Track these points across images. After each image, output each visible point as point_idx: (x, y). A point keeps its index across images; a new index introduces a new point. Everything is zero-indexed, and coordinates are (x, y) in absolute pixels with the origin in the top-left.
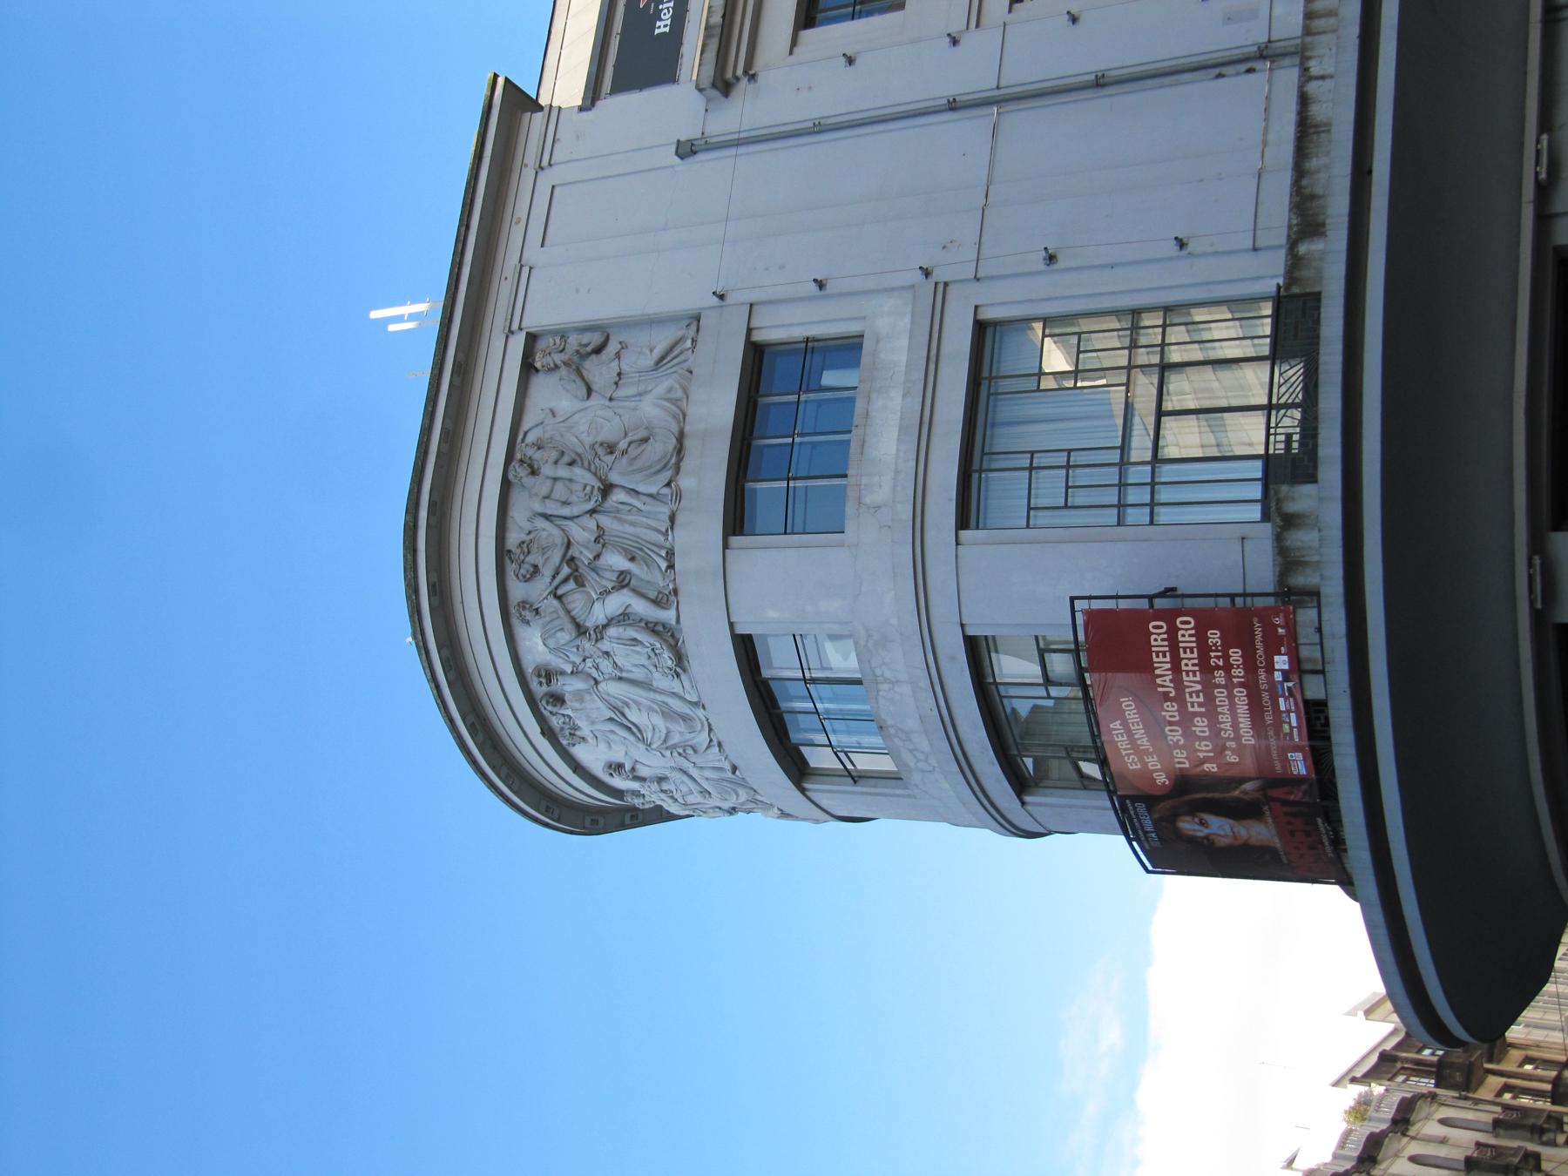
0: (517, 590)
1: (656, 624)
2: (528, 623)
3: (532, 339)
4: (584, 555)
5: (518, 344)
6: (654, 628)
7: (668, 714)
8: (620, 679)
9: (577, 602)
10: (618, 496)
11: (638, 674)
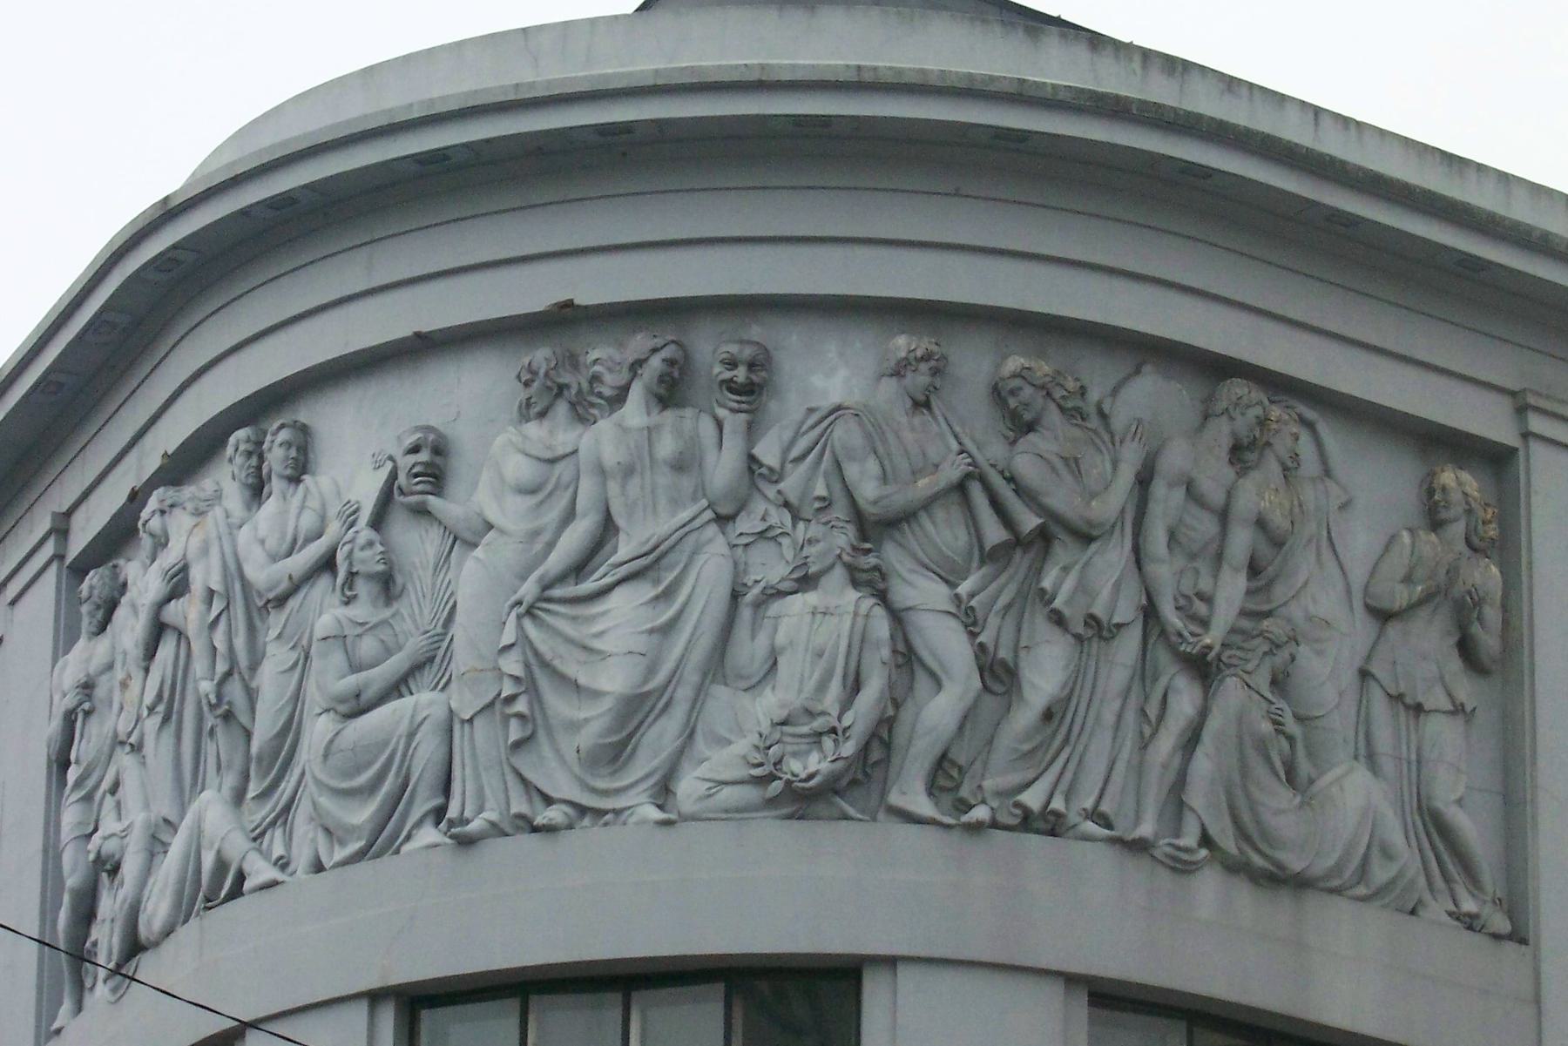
0: (975, 363)
1: (887, 746)
3: (1496, 460)
4: (1059, 578)
5: (1486, 419)
7: (636, 711)
10: (1185, 699)
11: (748, 650)
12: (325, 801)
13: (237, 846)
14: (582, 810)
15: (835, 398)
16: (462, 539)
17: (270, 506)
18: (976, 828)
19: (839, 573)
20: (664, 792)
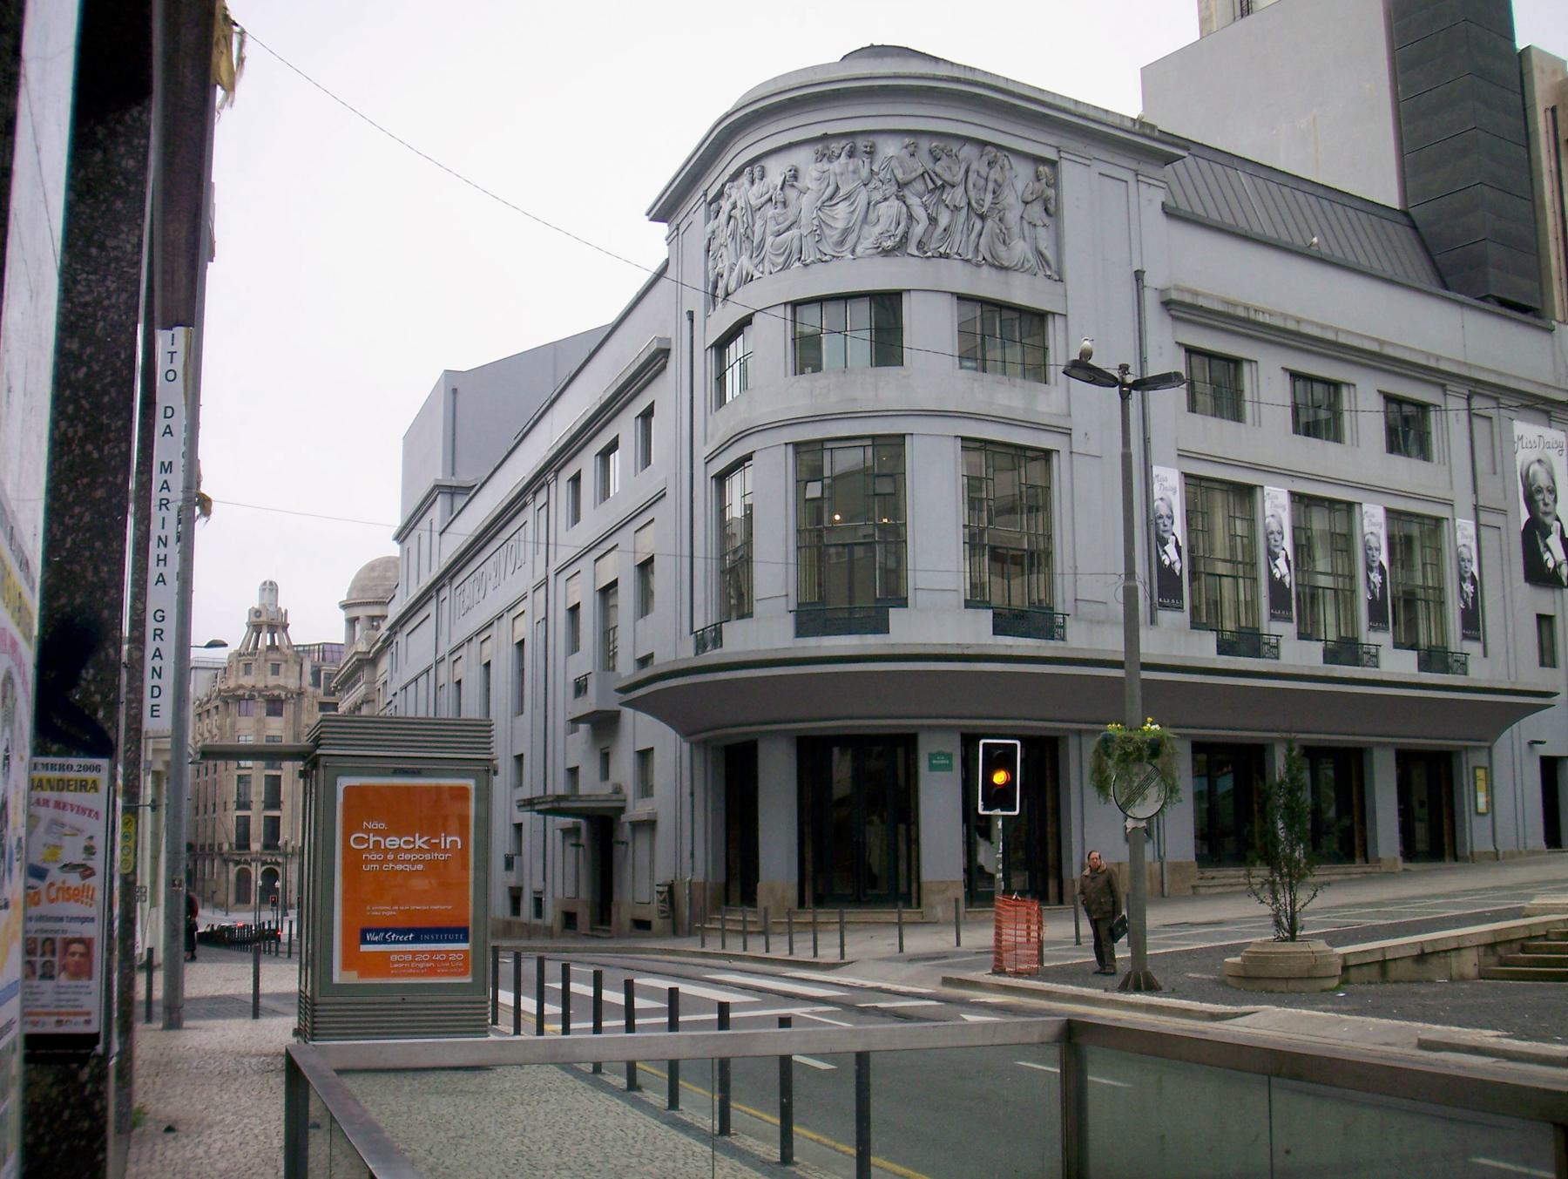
0: (925, 145)
3: (1053, 164)
5: (1050, 154)
6: (905, 237)
7: (846, 232)
11: (872, 217)
13: (751, 269)
20: (853, 252)
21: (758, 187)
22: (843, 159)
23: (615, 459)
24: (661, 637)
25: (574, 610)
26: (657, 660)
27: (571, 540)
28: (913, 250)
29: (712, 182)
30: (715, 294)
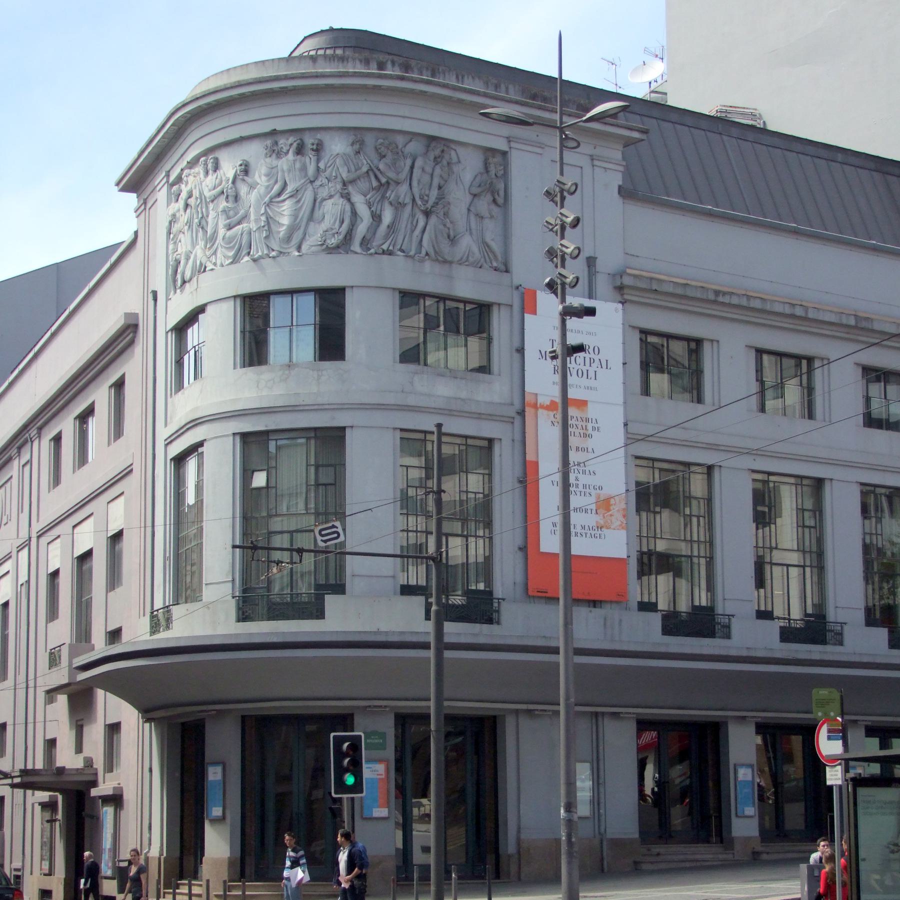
2: (352, 144)
3: (504, 154)
4: (391, 195)
5: (502, 145)
6: (349, 237)
8: (315, 201)
9: (363, 185)
11: (318, 214)
12: (223, 250)
13: (204, 260)
14: (281, 252)
15: (337, 152)
16: (252, 187)
17: (210, 177)
18: (371, 254)
19: (338, 195)
20: (299, 249)
21: (211, 179)
22: (291, 156)
23: (93, 424)
24: (129, 615)
25: (55, 574)
26: (125, 636)
27: (54, 504)
28: (356, 247)
29: (176, 163)
30: (177, 280)
